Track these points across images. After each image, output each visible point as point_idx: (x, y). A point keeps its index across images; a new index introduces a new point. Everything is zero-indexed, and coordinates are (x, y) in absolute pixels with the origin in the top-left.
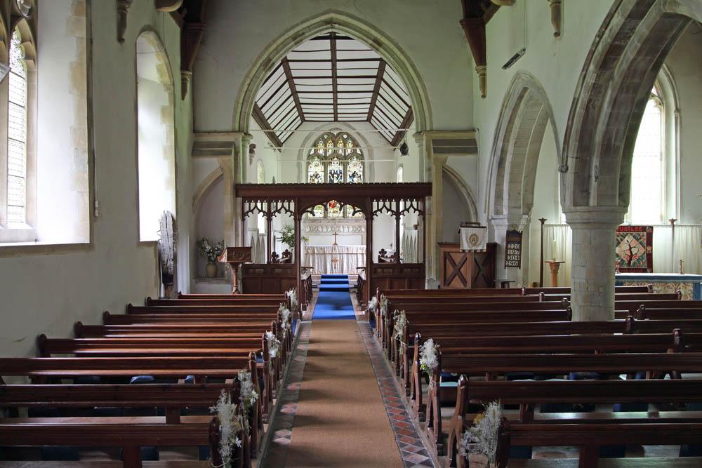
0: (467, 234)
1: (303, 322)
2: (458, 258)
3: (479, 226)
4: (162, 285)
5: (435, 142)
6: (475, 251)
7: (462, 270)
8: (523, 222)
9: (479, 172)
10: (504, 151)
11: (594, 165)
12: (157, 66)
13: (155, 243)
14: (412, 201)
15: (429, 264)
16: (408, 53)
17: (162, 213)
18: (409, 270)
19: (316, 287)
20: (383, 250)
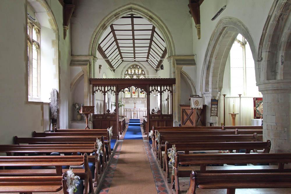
0: (193, 100)
1: (120, 141)
2: (189, 112)
3: (197, 96)
4: (52, 124)
5: (176, 60)
6: (198, 108)
7: (191, 117)
8: (218, 95)
9: (198, 74)
10: (210, 62)
11: (280, 55)
12: (49, 20)
13: (49, 104)
14: (167, 87)
15: (175, 114)
16: (165, 22)
17: (52, 90)
18: (166, 117)
19: (127, 124)
20: (153, 109)
